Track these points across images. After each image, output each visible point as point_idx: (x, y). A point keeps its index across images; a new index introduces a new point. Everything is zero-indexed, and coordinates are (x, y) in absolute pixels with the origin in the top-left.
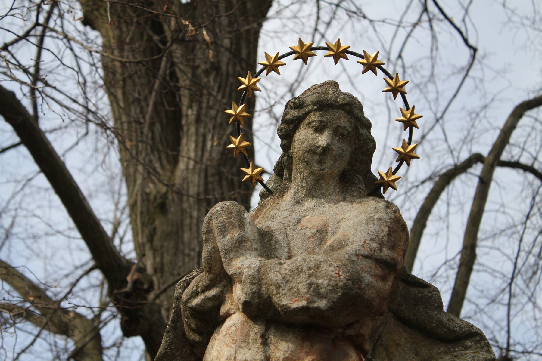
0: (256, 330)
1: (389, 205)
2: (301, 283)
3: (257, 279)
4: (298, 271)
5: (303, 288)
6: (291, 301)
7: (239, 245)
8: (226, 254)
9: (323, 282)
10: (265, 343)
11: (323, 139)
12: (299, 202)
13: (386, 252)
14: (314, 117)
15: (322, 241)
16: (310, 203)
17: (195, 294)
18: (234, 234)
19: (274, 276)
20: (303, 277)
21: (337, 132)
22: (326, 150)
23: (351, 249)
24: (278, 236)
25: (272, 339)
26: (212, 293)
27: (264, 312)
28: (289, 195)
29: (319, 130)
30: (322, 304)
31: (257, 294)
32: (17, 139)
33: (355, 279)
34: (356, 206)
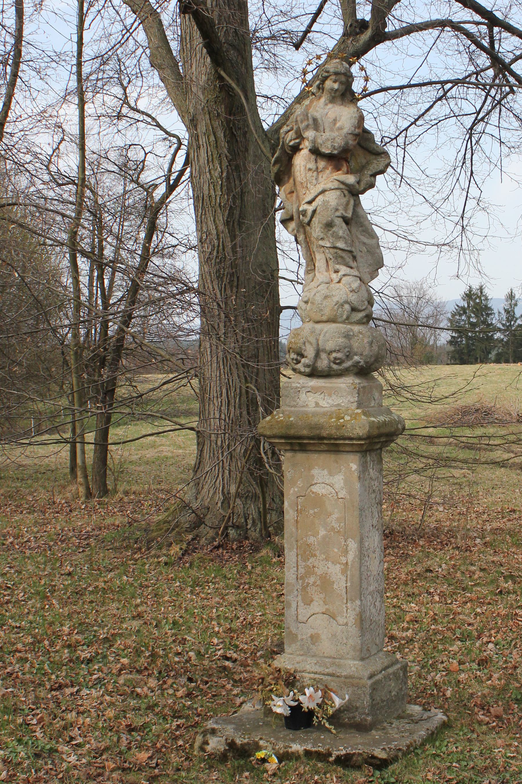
0: (313, 157)
1: (358, 108)
2: (329, 144)
3: (314, 141)
4: (328, 140)
5: (329, 146)
6: (326, 150)
7: (307, 127)
8: (412, 621)
9: (336, 145)
10: (316, 162)
11: (336, 86)
12: (326, 105)
13: (357, 130)
14: (333, 77)
15: (335, 124)
16: (330, 106)
17: (291, 141)
18: (305, 123)
19: (320, 141)
20: (329, 143)
21: (341, 83)
22: (337, 90)
23: (345, 131)
24: (320, 121)
25: (319, 160)
26: (297, 141)
27: (315, 152)
28: (323, 100)
29: (335, 82)
30: (335, 152)
31: (314, 146)
32: (280, 281)
33: (347, 144)
34: (346, 109)
